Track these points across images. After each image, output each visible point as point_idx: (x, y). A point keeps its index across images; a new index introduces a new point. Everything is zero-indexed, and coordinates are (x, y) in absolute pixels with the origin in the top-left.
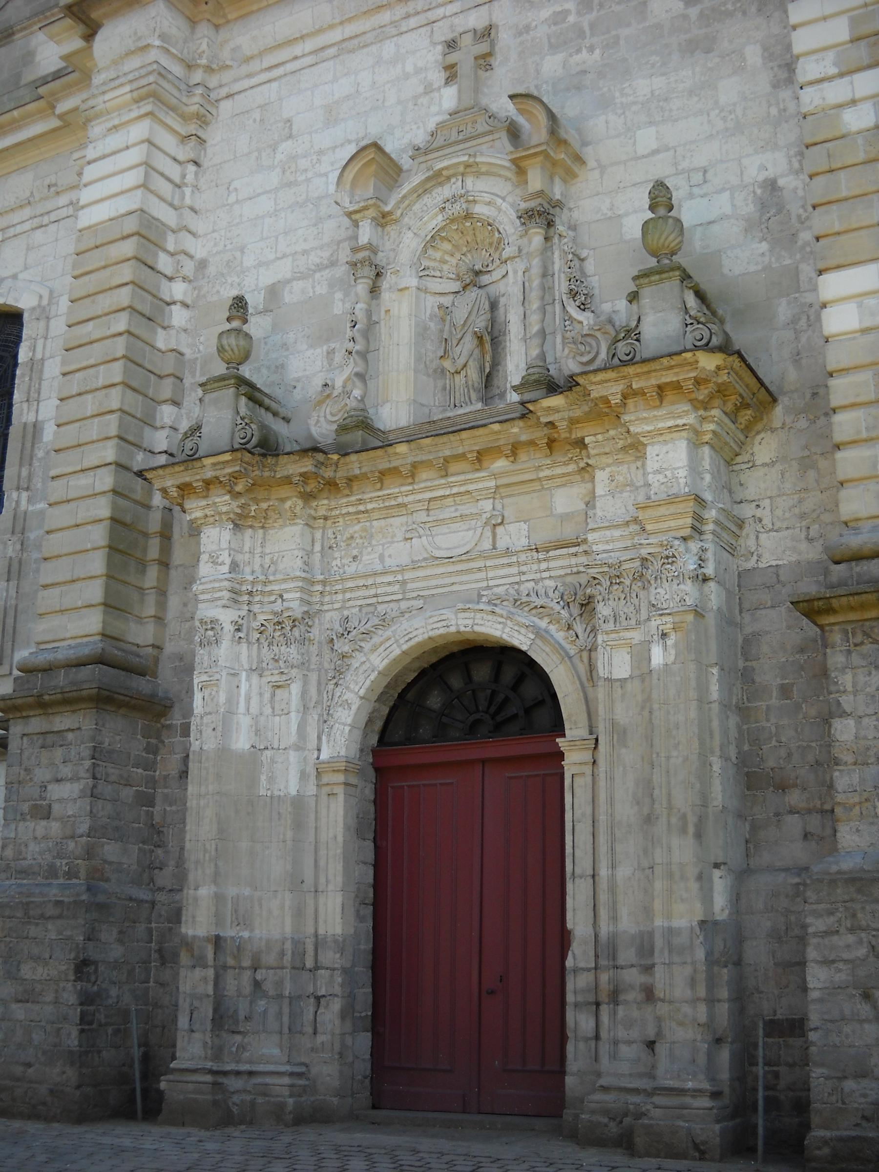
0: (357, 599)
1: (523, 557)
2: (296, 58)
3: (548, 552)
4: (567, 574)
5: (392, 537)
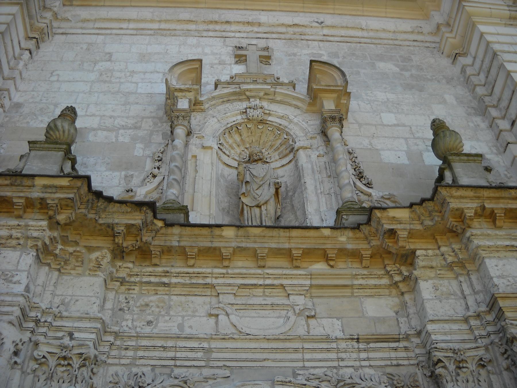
0: (151, 358)
1: (343, 345)
2: (121, 29)
3: (368, 343)
4: (387, 366)
5: (193, 312)
